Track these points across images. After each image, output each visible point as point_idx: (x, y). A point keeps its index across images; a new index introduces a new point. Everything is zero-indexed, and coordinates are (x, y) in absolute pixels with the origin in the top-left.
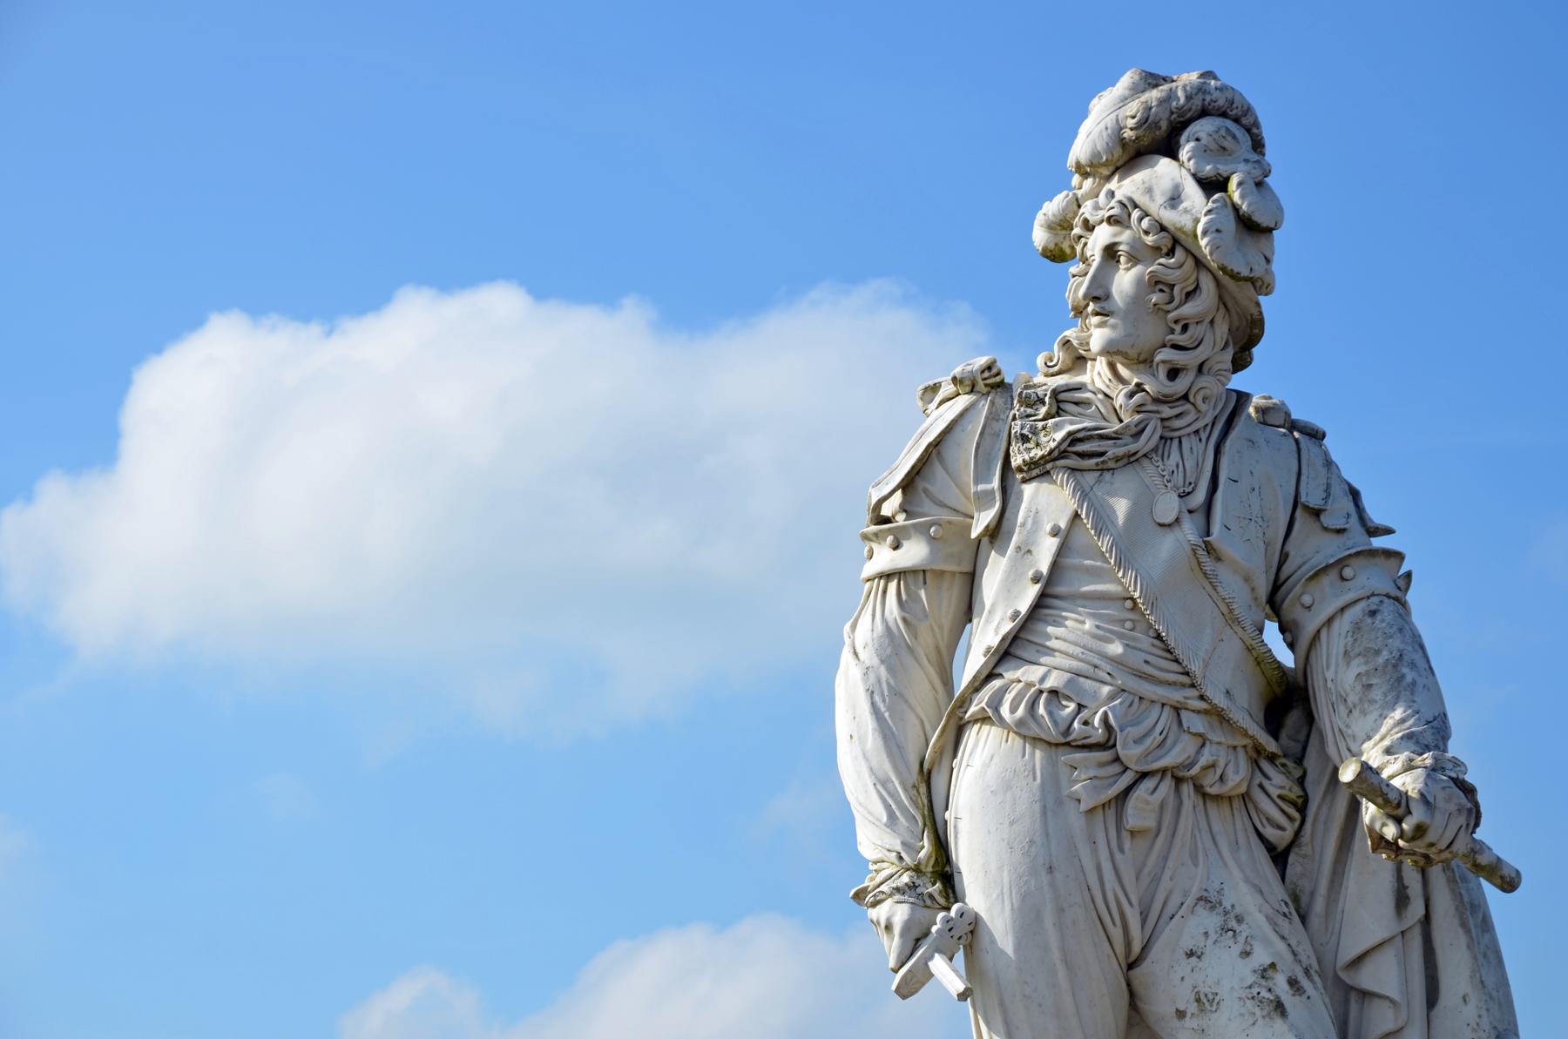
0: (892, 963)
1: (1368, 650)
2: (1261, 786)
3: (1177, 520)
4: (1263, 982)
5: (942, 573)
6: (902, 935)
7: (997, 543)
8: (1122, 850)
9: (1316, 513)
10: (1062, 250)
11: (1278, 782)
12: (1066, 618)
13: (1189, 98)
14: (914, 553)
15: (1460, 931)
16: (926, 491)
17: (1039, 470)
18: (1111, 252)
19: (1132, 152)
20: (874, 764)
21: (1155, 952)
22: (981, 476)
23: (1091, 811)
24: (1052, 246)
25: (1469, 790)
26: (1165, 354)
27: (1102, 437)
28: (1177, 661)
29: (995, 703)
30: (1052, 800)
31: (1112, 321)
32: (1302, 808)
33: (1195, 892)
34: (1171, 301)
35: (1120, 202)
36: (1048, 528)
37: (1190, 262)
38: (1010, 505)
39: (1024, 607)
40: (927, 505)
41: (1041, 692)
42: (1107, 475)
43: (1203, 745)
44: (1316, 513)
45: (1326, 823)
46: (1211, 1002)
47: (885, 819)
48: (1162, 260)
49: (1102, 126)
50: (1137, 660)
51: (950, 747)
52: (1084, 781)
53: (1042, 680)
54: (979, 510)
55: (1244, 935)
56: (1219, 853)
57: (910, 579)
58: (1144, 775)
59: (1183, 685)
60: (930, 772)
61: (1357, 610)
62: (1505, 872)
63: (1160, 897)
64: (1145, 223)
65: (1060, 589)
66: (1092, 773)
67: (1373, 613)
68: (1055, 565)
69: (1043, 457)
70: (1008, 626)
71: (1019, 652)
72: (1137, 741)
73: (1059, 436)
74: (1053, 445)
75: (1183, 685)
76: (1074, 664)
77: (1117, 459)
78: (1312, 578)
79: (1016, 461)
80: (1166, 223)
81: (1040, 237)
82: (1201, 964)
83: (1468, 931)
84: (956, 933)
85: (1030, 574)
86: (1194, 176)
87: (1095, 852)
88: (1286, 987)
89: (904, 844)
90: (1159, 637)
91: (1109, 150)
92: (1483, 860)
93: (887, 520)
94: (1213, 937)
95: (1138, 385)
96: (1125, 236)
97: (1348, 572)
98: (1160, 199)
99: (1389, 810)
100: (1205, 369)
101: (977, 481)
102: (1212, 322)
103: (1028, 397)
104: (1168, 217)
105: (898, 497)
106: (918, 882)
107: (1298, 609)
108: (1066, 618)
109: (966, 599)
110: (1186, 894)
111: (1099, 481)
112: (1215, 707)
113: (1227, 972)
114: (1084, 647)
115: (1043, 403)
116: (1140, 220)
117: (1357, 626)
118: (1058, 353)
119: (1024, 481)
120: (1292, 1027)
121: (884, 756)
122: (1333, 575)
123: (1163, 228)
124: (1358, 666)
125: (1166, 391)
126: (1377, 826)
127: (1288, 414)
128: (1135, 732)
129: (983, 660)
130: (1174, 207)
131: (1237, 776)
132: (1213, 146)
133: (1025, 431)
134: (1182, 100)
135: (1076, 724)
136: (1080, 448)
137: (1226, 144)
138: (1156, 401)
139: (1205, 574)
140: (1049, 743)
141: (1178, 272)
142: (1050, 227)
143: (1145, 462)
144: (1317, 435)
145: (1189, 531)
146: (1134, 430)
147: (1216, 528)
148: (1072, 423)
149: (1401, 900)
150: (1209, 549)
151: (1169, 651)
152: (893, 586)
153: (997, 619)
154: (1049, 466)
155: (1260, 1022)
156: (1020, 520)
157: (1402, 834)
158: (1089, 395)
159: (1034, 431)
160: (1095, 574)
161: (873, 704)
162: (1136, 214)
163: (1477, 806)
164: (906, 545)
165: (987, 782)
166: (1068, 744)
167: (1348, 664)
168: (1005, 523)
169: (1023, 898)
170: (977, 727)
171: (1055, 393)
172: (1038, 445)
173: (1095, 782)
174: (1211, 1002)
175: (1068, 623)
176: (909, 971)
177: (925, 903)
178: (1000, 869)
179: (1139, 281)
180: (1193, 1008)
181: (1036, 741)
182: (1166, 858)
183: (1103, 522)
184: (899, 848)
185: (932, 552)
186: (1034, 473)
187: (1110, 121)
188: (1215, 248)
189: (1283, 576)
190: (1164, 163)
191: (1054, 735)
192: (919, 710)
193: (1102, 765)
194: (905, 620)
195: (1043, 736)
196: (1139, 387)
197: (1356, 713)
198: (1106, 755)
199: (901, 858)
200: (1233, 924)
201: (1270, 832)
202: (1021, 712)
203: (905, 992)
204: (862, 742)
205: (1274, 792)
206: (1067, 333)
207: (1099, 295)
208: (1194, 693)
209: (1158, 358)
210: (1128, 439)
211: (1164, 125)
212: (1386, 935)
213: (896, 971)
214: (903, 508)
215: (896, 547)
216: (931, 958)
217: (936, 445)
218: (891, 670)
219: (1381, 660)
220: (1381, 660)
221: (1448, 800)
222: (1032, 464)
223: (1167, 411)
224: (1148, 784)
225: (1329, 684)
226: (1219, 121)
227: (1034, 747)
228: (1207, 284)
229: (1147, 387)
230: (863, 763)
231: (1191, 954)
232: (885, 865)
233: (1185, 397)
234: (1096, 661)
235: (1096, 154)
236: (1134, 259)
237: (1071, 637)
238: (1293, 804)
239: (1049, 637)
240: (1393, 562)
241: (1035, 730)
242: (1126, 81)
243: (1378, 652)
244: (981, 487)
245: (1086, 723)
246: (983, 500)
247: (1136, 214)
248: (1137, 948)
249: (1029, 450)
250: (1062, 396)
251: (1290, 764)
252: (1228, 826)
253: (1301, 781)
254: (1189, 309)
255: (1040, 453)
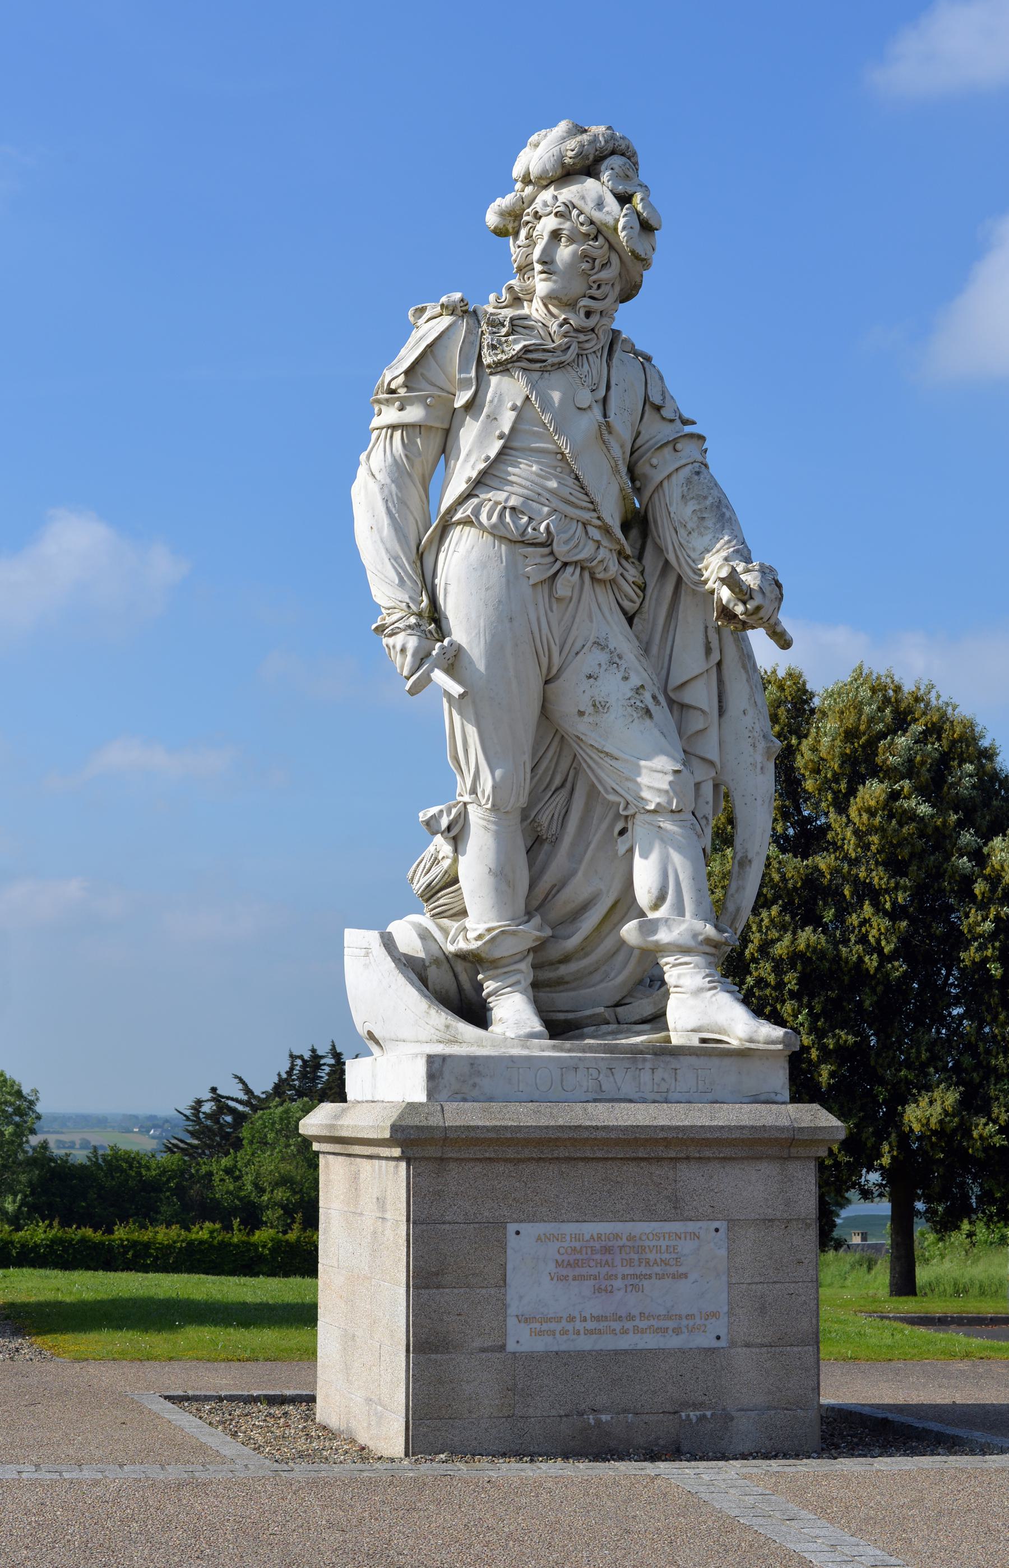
0: (405, 673)
1: (699, 496)
2: (622, 575)
3: (590, 407)
4: (637, 696)
5: (431, 427)
6: (414, 655)
7: (471, 412)
8: (552, 611)
9: (658, 409)
10: (507, 230)
11: (632, 573)
12: (520, 463)
13: (606, 142)
14: (414, 414)
15: (742, 671)
16: (422, 374)
17: (502, 368)
18: (555, 235)
19: (566, 174)
20: (388, 546)
21: (565, 675)
22: (463, 368)
23: (534, 585)
24: (501, 226)
25: (779, 586)
26: (585, 302)
27: (544, 350)
28: (586, 494)
29: (477, 512)
30: (512, 576)
31: (554, 278)
32: (643, 588)
33: (592, 639)
34: (593, 269)
35: (564, 203)
36: (510, 405)
37: (607, 246)
38: (481, 388)
39: (493, 454)
40: (423, 384)
41: (505, 508)
42: (546, 375)
43: (598, 548)
44: (658, 409)
45: (657, 600)
46: (604, 707)
47: (397, 581)
48: (590, 243)
49: (550, 153)
50: (565, 492)
51: (437, 538)
52: (534, 566)
53: (506, 500)
54: (460, 390)
55: (624, 667)
56: (603, 615)
57: (410, 430)
58: (565, 564)
59: (589, 510)
60: (422, 553)
61: (686, 472)
62: (787, 638)
63: (570, 641)
64: (582, 218)
65: (515, 444)
66: (538, 561)
67: (698, 473)
68: (513, 429)
69: (506, 360)
70: (482, 465)
71: (488, 482)
72: (566, 542)
73: (518, 347)
74: (514, 353)
75: (589, 510)
76: (525, 492)
77: (552, 365)
78: (658, 448)
79: (487, 360)
80: (594, 219)
81: (492, 219)
82: (596, 683)
83: (747, 672)
84: (447, 656)
85: (497, 433)
86: (611, 191)
87: (537, 609)
88: (651, 700)
89: (410, 598)
90: (577, 478)
91: (554, 169)
92: (778, 630)
93: (393, 392)
94: (604, 667)
95: (564, 319)
96: (567, 225)
97: (679, 446)
98: (591, 205)
99: (739, 596)
100: (604, 314)
101: (460, 372)
102: (613, 285)
103: (494, 320)
104: (596, 215)
105: (401, 379)
106: (421, 623)
107: (648, 466)
108: (520, 463)
109: (442, 445)
110: (587, 640)
111: (541, 378)
112: (605, 524)
113: (614, 688)
114: (532, 482)
115: (504, 326)
116: (578, 216)
117: (689, 481)
118: (505, 295)
119: (491, 374)
120: (656, 725)
121: (396, 542)
122: (670, 447)
123: (592, 223)
124: (692, 506)
125: (584, 325)
126: (731, 606)
127: (633, 345)
128: (565, 536)
129: (466, 486)
130: (600, 210)
131: (614, 569)
132: (622, 174)
133: (494, 342)
134: (603, 143)
135: (530, 530)
136: (530, 356)
137: (629, 173)
138: (576, 330)
139: (604, 442)
140: (510, 541)
141: (600, 251)
142: (502, 214)
143: (569, 368)
144: (648, 359)
145: (597, 412)
146: (564, 347)
147: (611, 413)
148: (525, 340)
149: (708, 651)
150: (608, 425)
151: (582, 488)
152: (398, 434)
153: (472, 460)
154: (509, 366)
155: (636, 721)
156: (489, 397)
157: (746, 612)
158: (533, 323)
159: (500, 343)
160: (539, 437)
161: (388, 508)
162: (575, 212)
163: (782, 595)
164: (409, 408)
165: (462, 565)
166: (523, 542)
167: (686, 504)
168: (478, 399)
169: (493, 636)
170: (459, 528)
171: (512, 319)
172: (503, 352)
173: (541, 567)
174: (604, 707)
175: (521, 466)
176: (418, 678)
177: (425, 635)
178: (479, 617)
179: (574, 254)
180: (590, 710)
181: (502, 538)
182: (574, 617)
183: (546, 404)
184: (408, 601)
185: (427, 414)
186: (499, 369)
187: (555, 151)
188: (630, 239)
189: (636, 446)
190: (590, 182)
191: (516, 535)
192: (415, 514)
193: (543, 556)
194: (406, 456)
195: (509, 536)
196: (566, 321)
197: (695, 534)
198: (546, 550)
199: (409, 607)
200: (616, 659)
201: (626, 604)
202: (495, 518)
203: (413, 691)
204: (380, 531)
205: (631, 579)
206: (512, 282)
207: (547, 261)
208: (594, 515)
209: (582, 303)
210: (559, 353)
211: (591, 157)
212: (701, 671)
213: (408, 678)
214: (405, 385)
215: (401, 409)
216: (432, 671)
217: (430, 346)
218: (398, 487)
219: (708, 503)
220: (708, 503)
221: (772, 592)
222: (499, 363)
223: (582, 337)
224: (570, 569)
225: (672, 515)
226: (624, 159)
227: (500, 543)
228: (615, 260)
229: (572, 322)
230: (381, 545)
231: (590, 677)
232: (396, 610)
233: (593, 330)
234: (540, 491)
235: (545, 171)
236: (571, 240)
237: (523, 474)
238: (639, 587)
239: (509, 474)
240: (700, 441)
241: (503, 532)
242: (563, 126)
243: (705, 498)
244: (462, 376)
245: (534, 529)
246: (464, 384)
247: (575, 212)
248: (554, 671)
249: (496, 355)
250: (515, 322)
251: (636, 562)
252: (605, 598)
253: (642, 573)
254: (604, 275)
255: (504, 358)
